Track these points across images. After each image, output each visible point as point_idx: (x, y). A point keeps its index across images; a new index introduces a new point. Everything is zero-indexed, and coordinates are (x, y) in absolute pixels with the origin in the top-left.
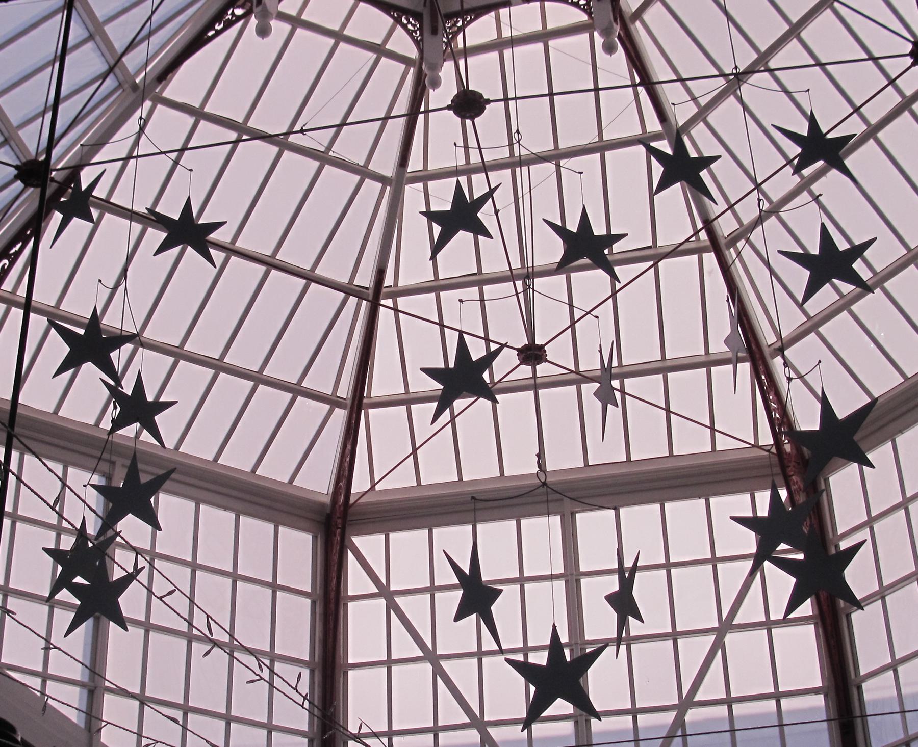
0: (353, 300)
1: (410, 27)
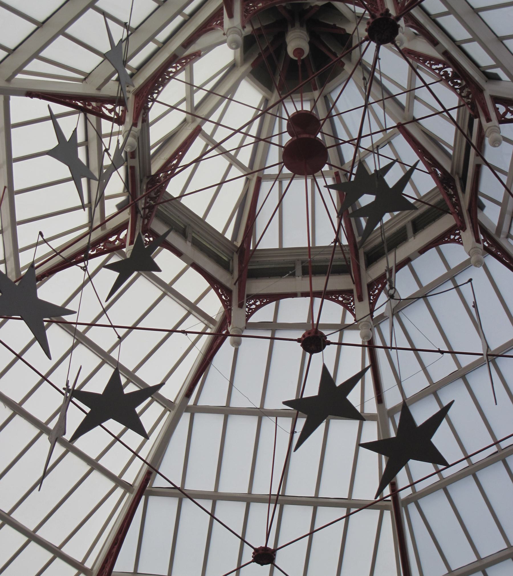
0: (120, 491)
1: (223, 297)
